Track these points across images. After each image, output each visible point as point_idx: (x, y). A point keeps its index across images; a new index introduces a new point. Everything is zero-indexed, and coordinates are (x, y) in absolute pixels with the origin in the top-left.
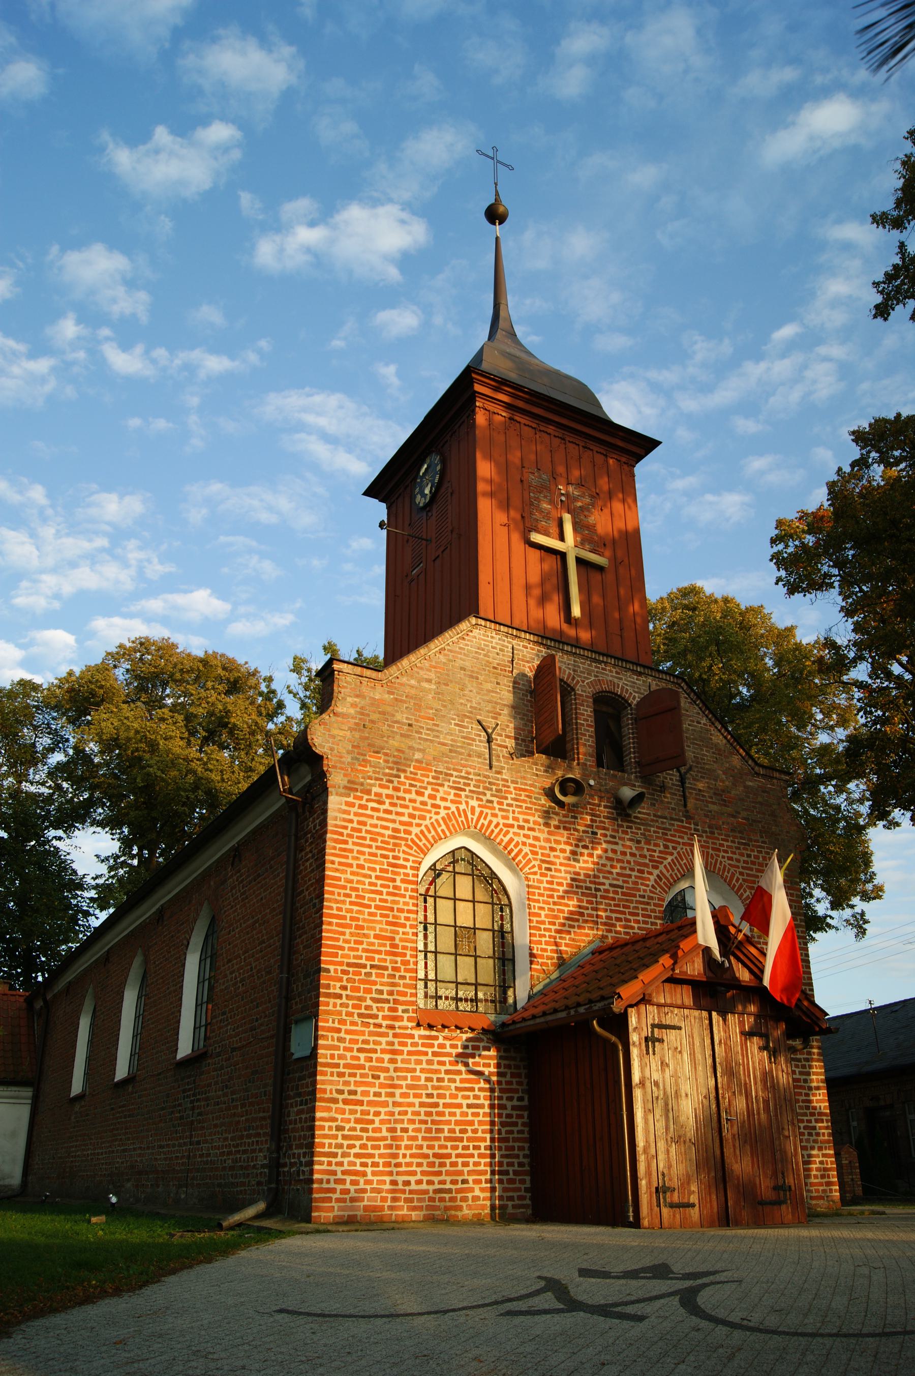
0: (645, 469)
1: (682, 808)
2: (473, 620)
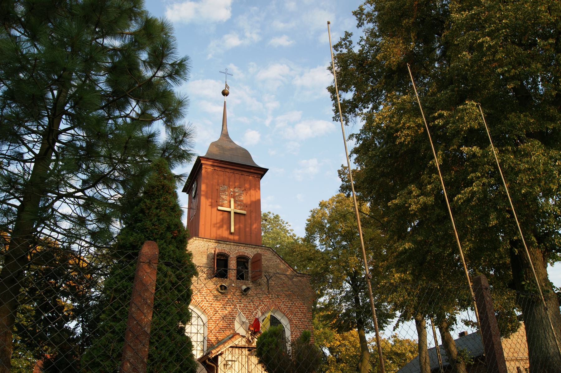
0: (264, 181)
1: (267, 290)
2: (195, 238)
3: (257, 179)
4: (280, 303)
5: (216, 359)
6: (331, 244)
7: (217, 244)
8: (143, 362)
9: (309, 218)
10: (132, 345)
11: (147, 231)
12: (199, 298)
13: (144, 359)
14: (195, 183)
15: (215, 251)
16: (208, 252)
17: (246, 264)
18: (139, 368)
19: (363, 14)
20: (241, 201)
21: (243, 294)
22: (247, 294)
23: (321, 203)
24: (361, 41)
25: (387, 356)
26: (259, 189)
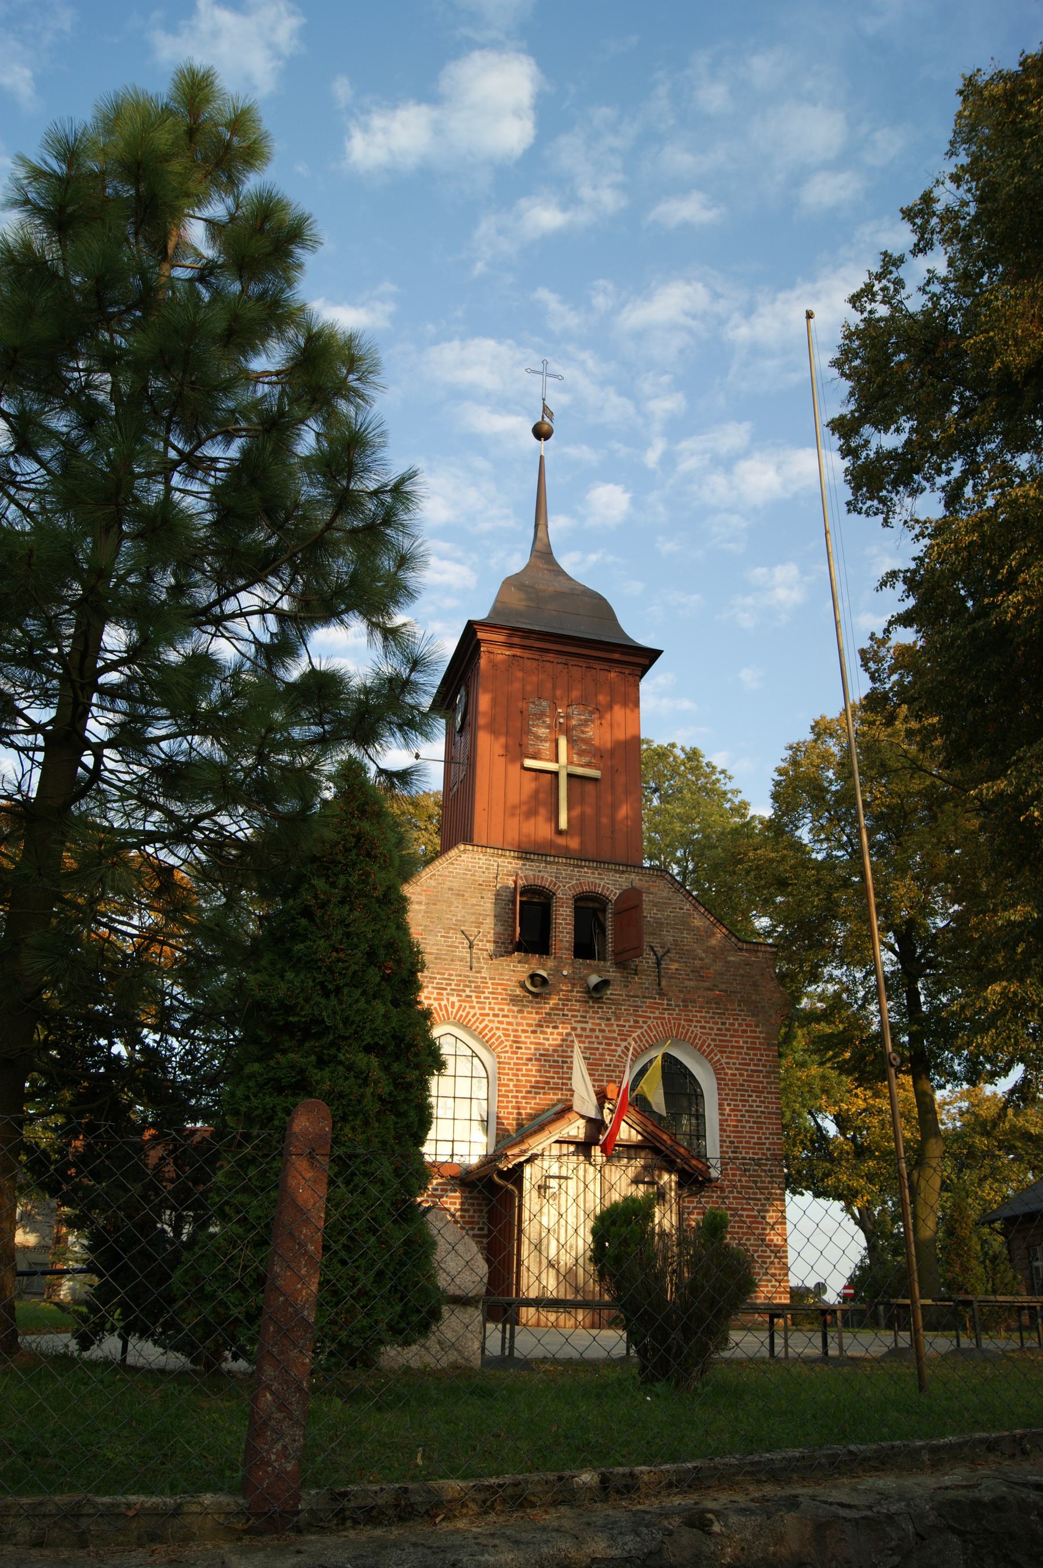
1: (656, 987)
2: (462, 847)
3: (631, 678)
4: (692, 1021)
5: (516, 1175)
6: (845, 838)
7: (521, 862)
8: (299, 1389)
9: (783, 765)
10: (275, 1350)
11: (320, 968)
12: (473, 1007)
13: (301, 1383)
14: (463, 691)
15: (515, 882)
16: (499, 885)
17: (600, 915)
18: (291, 1404)
19: (934, 214)
20: (587, 741)
21: (591, 997)
22: (601, 998)
23: (817, 723)
24: (928, 283)
25: (999, 1141)
26: (637, 704)
